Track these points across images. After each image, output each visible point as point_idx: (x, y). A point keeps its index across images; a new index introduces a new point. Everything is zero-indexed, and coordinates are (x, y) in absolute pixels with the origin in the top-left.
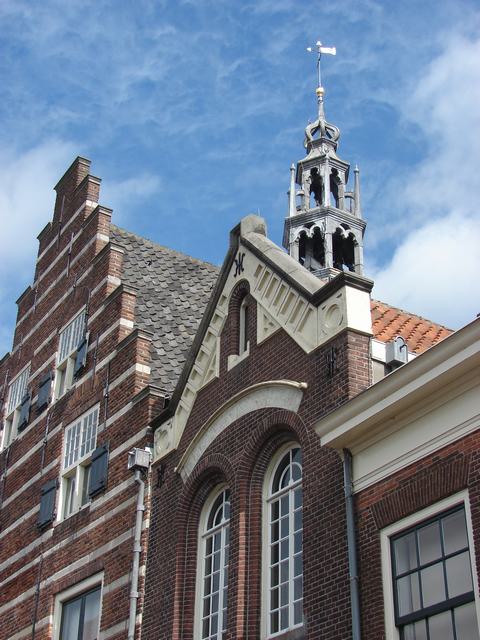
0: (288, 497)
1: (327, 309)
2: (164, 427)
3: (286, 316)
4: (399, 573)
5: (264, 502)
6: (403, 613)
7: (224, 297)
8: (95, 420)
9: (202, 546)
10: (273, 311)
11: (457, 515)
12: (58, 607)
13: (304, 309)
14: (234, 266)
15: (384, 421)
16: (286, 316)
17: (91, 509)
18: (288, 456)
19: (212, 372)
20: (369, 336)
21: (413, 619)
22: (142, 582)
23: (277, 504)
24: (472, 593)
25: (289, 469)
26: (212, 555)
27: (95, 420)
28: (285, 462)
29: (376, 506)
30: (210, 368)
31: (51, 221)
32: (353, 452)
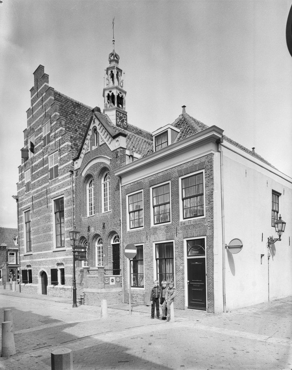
0: (107, 183)
1: (116, 140)
2: (76, 161)
3: (106, 139)
4: (154, 196)
5: (102, 184)
6: (130, 211)
7: (90, 129)
8: (57, 155)
9: (88, 191)
10: (103, 137)
11: (141, 193)
12: (24, 213)
13: (110, 139)
14: (93, 121)
15: (125, 173)
16: (106, 139)
17: (59, 179)
18: (107, 174)
19: (88, 149)
20: (125, 149)
21: (186, 198)
22: (22, 221)
23: (105, 184)
24: (170, 202)
25: (107, 177)
26: (90, 193)
27: (57, 155)
28: (106, 175)
29: (126, 189)
30: (88, 148)
31: (34, 86)
32: (121, 177)
